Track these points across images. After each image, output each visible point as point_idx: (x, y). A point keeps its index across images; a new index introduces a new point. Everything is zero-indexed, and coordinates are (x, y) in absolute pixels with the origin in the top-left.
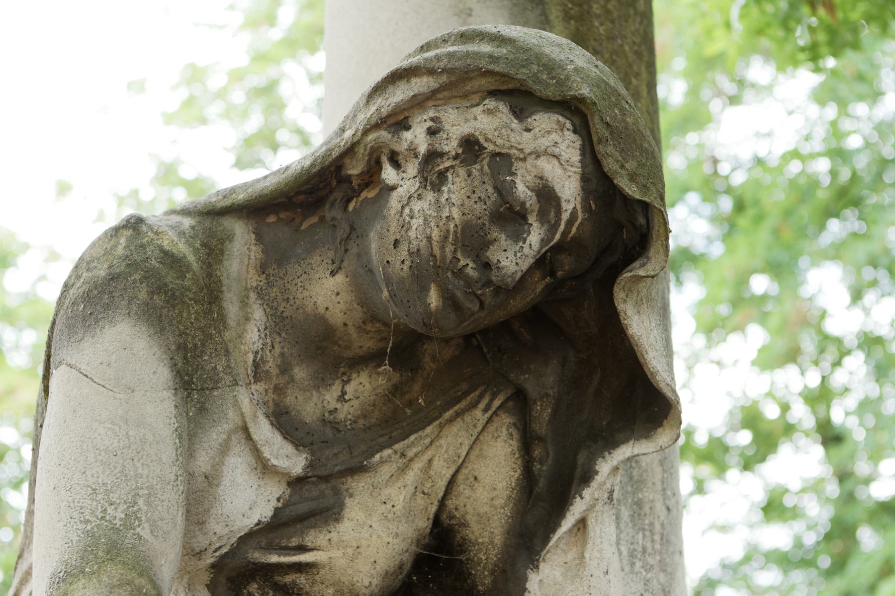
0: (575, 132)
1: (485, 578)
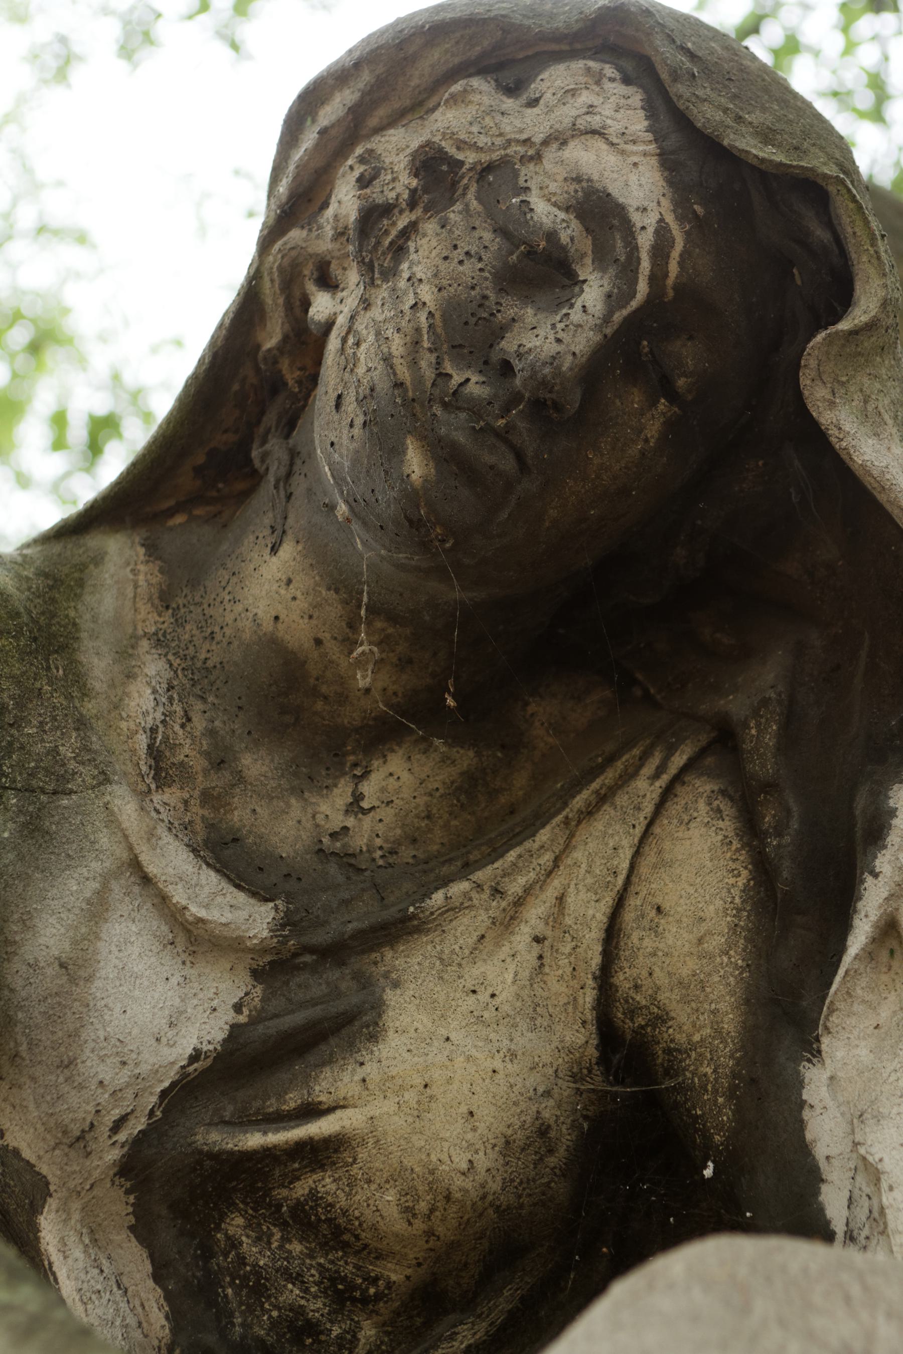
0: (627, 81)
1: (720, 1112)
